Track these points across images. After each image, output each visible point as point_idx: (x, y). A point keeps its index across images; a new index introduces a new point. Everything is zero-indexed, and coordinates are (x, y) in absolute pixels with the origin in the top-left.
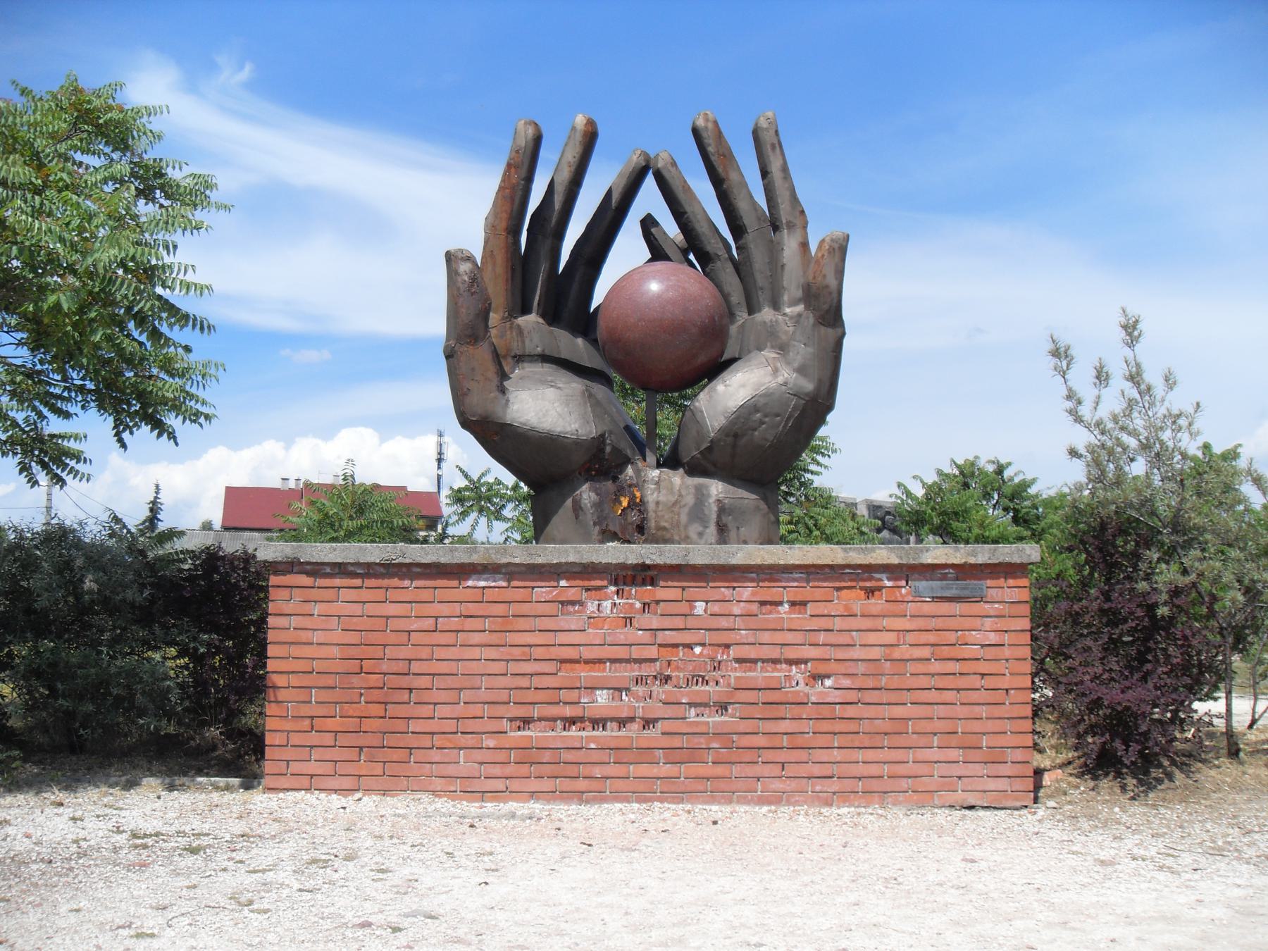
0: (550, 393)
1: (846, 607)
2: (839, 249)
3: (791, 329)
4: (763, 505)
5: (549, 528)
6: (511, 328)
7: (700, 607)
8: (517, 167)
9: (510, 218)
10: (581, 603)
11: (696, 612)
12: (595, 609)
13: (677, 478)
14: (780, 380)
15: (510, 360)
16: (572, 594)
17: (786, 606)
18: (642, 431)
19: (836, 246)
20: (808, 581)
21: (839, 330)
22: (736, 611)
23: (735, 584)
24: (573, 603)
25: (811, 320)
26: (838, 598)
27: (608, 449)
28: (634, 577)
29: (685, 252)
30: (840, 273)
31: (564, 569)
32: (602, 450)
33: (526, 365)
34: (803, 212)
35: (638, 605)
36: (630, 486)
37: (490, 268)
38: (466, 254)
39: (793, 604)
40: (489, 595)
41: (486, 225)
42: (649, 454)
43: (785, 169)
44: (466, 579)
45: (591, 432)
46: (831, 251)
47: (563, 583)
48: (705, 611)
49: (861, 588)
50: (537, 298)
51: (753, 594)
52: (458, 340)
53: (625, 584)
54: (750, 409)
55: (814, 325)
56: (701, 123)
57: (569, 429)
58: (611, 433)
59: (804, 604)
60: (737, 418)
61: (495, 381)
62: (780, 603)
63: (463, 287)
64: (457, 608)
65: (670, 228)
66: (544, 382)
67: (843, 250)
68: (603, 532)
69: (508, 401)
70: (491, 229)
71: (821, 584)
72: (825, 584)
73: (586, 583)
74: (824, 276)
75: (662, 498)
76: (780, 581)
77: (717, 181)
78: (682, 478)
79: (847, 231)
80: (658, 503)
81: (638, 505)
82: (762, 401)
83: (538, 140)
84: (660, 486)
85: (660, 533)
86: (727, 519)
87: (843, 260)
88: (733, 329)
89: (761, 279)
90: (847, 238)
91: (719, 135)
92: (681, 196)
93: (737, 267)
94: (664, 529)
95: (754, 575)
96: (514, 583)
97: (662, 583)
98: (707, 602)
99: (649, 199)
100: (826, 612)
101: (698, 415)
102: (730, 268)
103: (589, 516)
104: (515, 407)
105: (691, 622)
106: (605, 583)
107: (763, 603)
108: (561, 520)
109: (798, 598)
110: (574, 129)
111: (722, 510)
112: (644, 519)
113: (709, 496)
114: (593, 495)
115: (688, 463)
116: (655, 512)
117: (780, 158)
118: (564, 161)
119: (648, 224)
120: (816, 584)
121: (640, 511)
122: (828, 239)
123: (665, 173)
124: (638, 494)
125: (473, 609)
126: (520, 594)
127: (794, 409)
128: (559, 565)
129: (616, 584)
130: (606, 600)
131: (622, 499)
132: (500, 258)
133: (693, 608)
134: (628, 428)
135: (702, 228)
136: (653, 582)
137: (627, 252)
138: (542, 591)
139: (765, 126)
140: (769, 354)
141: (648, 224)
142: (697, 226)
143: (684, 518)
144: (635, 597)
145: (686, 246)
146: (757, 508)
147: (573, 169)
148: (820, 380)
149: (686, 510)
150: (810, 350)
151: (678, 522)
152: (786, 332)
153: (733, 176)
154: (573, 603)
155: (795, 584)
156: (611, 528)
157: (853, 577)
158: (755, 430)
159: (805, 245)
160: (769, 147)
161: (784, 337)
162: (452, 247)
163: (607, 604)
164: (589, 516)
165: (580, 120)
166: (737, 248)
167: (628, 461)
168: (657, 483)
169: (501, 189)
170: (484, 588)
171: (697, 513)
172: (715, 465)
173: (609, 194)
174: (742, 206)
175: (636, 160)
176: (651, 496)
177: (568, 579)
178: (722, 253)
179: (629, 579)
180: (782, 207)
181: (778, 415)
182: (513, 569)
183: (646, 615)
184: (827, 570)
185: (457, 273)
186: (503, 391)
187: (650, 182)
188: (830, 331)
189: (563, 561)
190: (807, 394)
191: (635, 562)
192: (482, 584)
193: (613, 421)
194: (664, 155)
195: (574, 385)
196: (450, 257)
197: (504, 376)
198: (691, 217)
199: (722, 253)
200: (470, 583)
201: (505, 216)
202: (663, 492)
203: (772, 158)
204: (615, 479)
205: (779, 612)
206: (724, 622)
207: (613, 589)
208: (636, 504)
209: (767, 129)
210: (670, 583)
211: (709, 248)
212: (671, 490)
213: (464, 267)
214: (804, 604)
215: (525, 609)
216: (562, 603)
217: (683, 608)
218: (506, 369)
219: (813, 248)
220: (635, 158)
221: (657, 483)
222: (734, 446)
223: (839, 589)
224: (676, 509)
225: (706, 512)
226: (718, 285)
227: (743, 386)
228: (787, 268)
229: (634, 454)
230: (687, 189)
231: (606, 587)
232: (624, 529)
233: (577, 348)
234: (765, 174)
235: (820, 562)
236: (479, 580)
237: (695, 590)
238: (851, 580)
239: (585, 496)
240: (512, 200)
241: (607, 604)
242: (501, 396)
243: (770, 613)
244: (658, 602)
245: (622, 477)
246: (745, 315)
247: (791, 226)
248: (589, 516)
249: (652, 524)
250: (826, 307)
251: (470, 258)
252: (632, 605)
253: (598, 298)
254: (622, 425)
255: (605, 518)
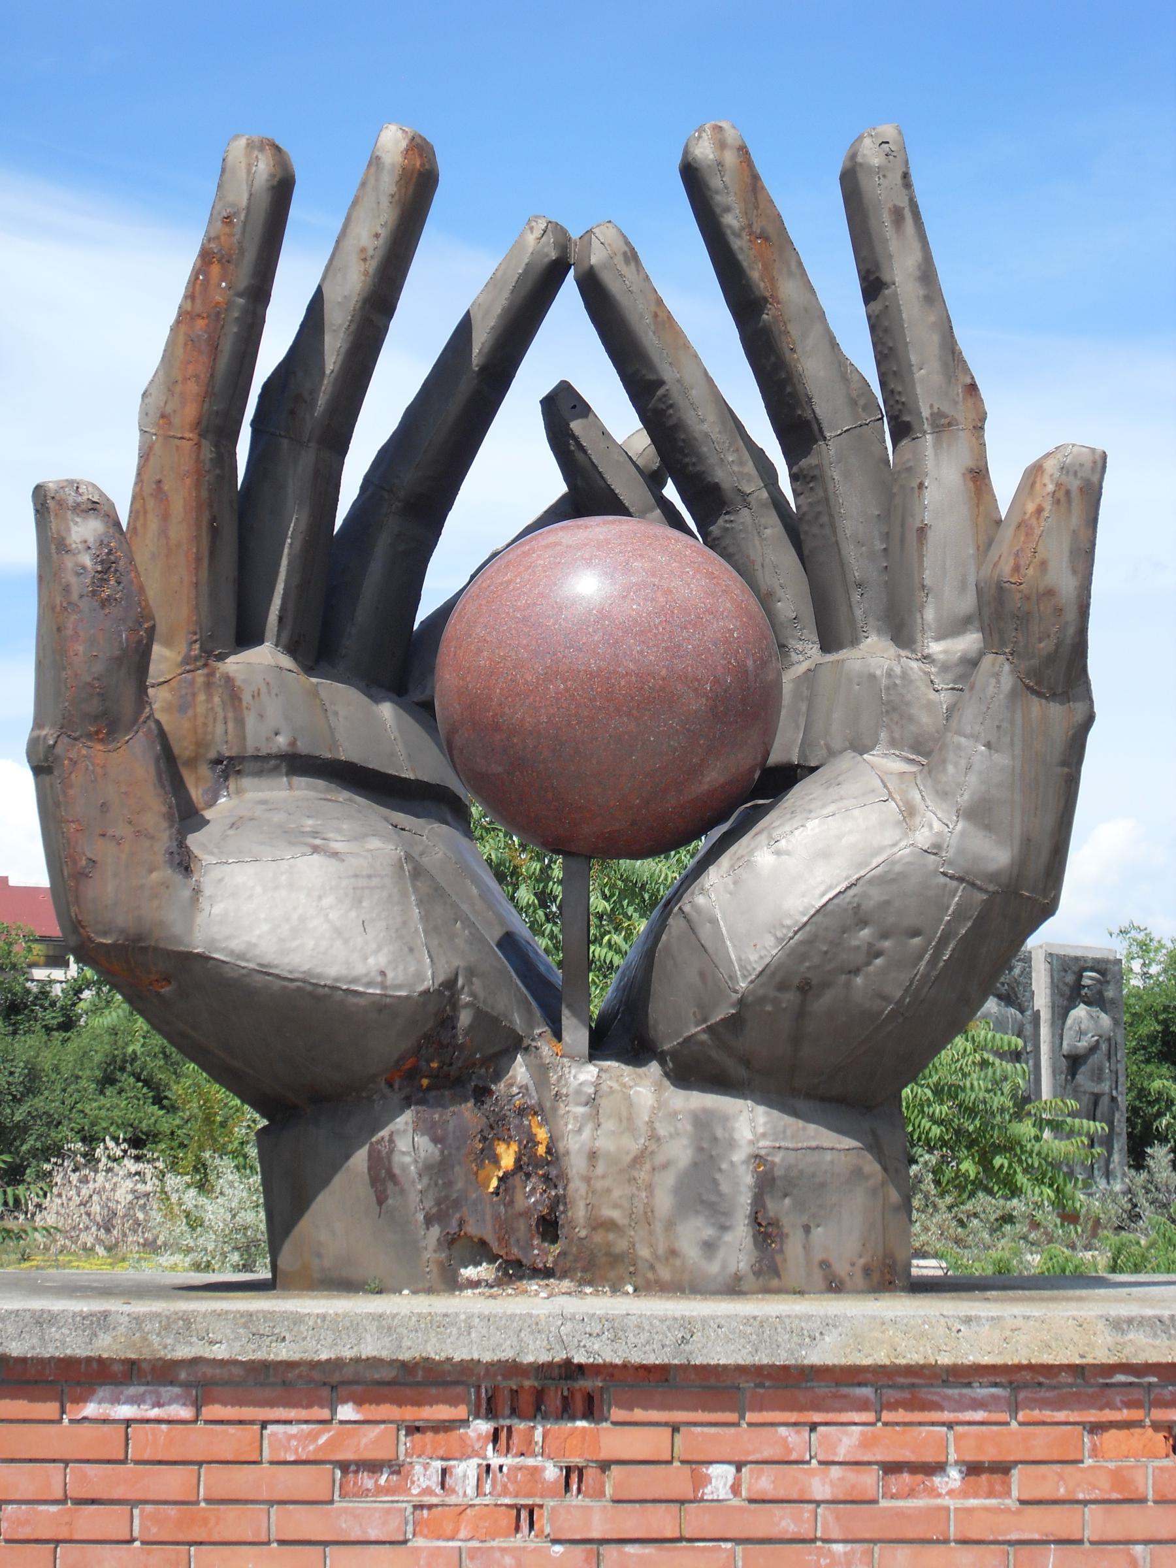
0: (312, 869)
1: (1118, 1478)
2: (1077, 491)
3: (944, 699)
4: (871, 1166)
5: (305, 1224)
6: (208, 685)
7: (720, 1478)
8: (226, 260)
9: (209, 394)
10: (396, 1467)
11: (709, 1492)
12: (434, 1481)
13: (643, 1088)
14: (923, 838)
15: (204, 770)
16: (369, 1442)
17: (954, 1474)
18: (551, 963)
19: (1075, 484)
20: (1014, 1408)
21: (1080, 707)
22: (820, 1489)
23: (817, 1417)
24: (374, 1467)
25: (1007, 681)
26: (1094, 1452)
27: (465, 1018)
28: (539, 1396)
29: (654, 481)
30: (1084, 556)
31: (348, 1373)
32: (447, 1022)
33: (246, 782)
34: (972, 388)
35: (552, 1473)
36: (522, 1112)
37: (153, 525)
38: (87, 494)
39: (973, 1469)
40: (143, 1443)
41: (144, 413)
42: (568, 1021)
43: (928, 275)
44: (83, 1399)
45: (419, 976)
46: (1062, 497)
47: (346, 1412)
48: (735, 1489)
49: (1156, 1426)
50: (284, 562)
51: (865, 1443)
52: (66, 727)
53: (514, 1412)
54: (843, 916)
55: (1013, 695)
56: (704, 151)
57: (360, 969)
58: (471, 972)
59: (1002, 1469)
60: (809, 942)
61: (164, 838)
62: (938, 1468)
63: (77, 585)
64: (54, 1479)
65: (618, 419)
66: (293, 836)
67: (1092, 494)
68: (450, 1241)
69: (197, 891)
70: (158, 425)
71: (1048, 1415)
72: (1061, 1416)
73: (410, 1413)
74: (1044, 564)
75: (605, 1143)
76: (938, 1407)
77: (747, 305)
78: (658, 1089)
79: (1100, 446)
80: (593, 1156)
81: (542, 1165)
82: (877, 895)
83: (282, 190)
84: (605, 1114)
85: (598, 1238)
86: (780, 1207)
87: (1092, 522)
88: (788, 679)
89: (858, 559)
90: (1101, 463)
91: (754, 184)
92: (650, 340)
93: (794, 529)
94: (610, 1225)
95: (867, 1392)
96: (214, 1411)
97: (617, 1414)
98: (739, 1466)
99: (566, 350)
100: (1062, 1492)
101: (705, 932)
102: (773, 528)
103: (415, 1197)
104: (218, 909)
105: (695, 1521)
106: (461, 1412)
107: (891, 1468)
108: (337, 1215)
109: (989, 1455)
110: (375, 161)
111: (768, 1183)
112: (557, 1201)
113: (732, 1144)
114: (424, 1142)
115: (674, 1054)
116: (588, 1180)
117: (916, 245)
118: (350, 244)
119: (562, 410)
120: (1036, 1414)
121: (547, 1178)
122: (1051, 466)
123: (614, 286)
124: (542, 1134)
125: (97, 1479)
126: (229, 1442)
127: (959, 915)
128: (336, 1364)
129: (491, 1413)
130: (464, 1456)
131: (501, 1148)
132: (181, 498)
133: (701, 1481)
134: (509, 943)
135: (702, 424)
136: (591, 1409)
137: (512, 471)
138: (290, 1433)
139: (876, 161)
140: (885, 762)
141: (562, 410)
142: (690, 417)
143: (664, 1202)
144: (545, 1449)
145: (656, 463)
146: (857, 1174)
147: (373, 265)
148: (1027, 842)
149: (668, 1179)
150: (1002, 759)
151: (649, 1210)
152: (930, 706)
153: (788, 290)
154: (374, 1467)
155: (979, 1415)
156: (472, 1229)
157: (1137, 1394)
158: (856, 971)
159: (978, 476)
160: (886, 217)
161: (925, 719)
162: (52, 476)
163: (466, 1470)
164: (413, 1198)
165: (392, 141)
166: (794, 477)
167: (515, 1044)
168: (592, 1101)
169: (184, 317)
170: (128, 1422)
171: (700, 1190)
172: (747, 1063)
173: (465, 328)
174: (811, 369)
175: (534, 245)
176: (576, 1139)
177: (359, 1402)
178: (753, 486)
179: (526, 1401)
180: (919, 374)
181: (916, 933)
182: (209, 1371)
183: (575, 1500)
184: (1065, 1378)
185: (62, 546)
186: (184, 863)
187: (569, 295)
188: (1055, 709)
189: (348, 1354)
190: (993, 877)
191: (544, 1358)
192: (125, 1411)
193: (477, 938)
194: (606, 234)
195: (375, 843)
196: (47, 504)
197: (187, 817)
198: (676, 396)
199: (753, 486)
200: (91, 1409)
201: (193, 388)
202: (608, 1125)
203: (894, 246)
204: (482, 1094)
205: (934, 1493)
206: (785, 1522)
207: (483, 1427)
208: (538, 1163)
209: (881, 171)
210: (639, 1414)
211: (722, 476)
212: (628, 1122)
213: (84, 531)
214: (1002, 1469)
215: (241, 1480)
216: (344, 1466)
217: (676, 1480)
218: (196, 794)
219: (1005, 485)
220: (531, 239)
221: (592, 1101)
222: (801, 1014)
223: (1096, 1428)
224: (642, 1175)
225: (725, 1188)
226: (744, 570)
227: (825, 854)
228: (931, 535)
229: (531, 1026)
230: (665, 321)
231: (465, 1423)
232: (505, 1229)
233: (375, 727)
234: (873, 286)
235: (1047, 1359)
236: (116, 1401)
237: (705, 1432)
238: (1129, 1405)
239: (403, 1144)
240: (215, 348)
241: (466, 1470)
242: (178, 878)
243: (911, 1494)
244: (605, 1466)
245: (500, 1088)
246: (814, 650)
247: (942, 425)
248: (413, 1198)
249: (578, 1212)
250: (1046, 646)
251: (98, 507)
252: (536, 1471)
253: (440, 583)
254: (493, 936)
255: (457, 1204)
